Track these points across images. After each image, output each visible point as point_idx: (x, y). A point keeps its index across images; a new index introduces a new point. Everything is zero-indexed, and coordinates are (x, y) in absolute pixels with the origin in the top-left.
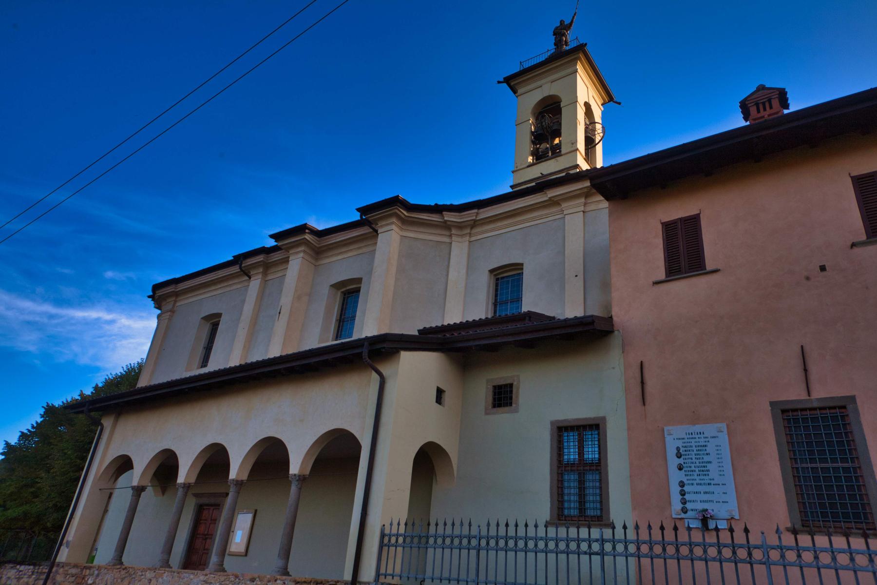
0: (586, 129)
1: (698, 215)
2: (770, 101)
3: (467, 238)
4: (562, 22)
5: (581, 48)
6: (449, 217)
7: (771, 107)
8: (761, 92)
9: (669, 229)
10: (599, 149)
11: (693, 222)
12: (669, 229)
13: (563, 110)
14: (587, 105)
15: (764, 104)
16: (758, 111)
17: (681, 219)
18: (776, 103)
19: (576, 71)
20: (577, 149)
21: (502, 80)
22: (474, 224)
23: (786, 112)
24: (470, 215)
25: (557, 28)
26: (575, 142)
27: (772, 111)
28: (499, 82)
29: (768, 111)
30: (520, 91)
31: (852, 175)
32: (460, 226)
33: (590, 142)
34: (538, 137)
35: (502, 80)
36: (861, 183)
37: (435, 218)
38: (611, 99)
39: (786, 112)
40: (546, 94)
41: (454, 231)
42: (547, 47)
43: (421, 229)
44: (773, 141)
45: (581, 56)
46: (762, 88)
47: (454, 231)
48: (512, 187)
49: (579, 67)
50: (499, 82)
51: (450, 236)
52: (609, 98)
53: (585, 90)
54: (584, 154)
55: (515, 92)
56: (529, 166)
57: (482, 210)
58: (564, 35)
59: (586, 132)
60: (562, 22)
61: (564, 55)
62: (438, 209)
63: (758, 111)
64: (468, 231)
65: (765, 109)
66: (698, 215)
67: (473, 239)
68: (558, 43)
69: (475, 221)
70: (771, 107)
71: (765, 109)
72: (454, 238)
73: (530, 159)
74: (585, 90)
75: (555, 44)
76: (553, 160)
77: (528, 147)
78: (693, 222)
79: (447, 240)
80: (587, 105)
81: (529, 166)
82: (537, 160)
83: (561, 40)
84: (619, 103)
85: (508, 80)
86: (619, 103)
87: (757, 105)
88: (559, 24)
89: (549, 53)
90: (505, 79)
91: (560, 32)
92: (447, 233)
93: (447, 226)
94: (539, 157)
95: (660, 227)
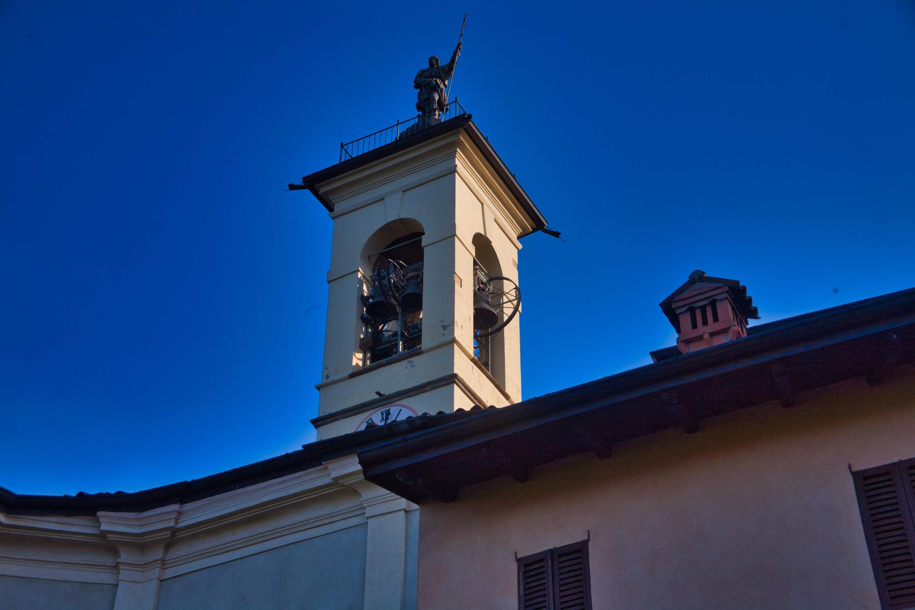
0: (478, 296)
1: (585, 543)
2: (713, 304)
3: (156, 572)
4: (432, 60)
5: (461, 122)
6: (112, 523)
7: (716, 319)
8: (696, 286)
9: (530, 567)
10: (512, 335)
11: (576, 555)
12: (530, 567)
13: (426, 252)
14: (482, 244)
15: (703, 309)
16: (695, 326)
17: (552, 552)
18: (726, 310)
19: (453, 171)
20: (454, 341)
21: (299, 182)
22: (173, 538)
23: (752, 323)
24: (162, 518)
25: (421, 74)
26: (448, 325)
27: (718, 326)
28: (292, 187)
29: (712, 326)
30: (339, 208)
31: (854, 469)
32: (140, 544)
33: (488, 323)
34: (375, 311)
35: (299, 182)
36: (872, 485)
37: (77, 526)
38: (538, 225)
39: (752, 323)
40: (392, 216)
41: (125, 556)
42: (406, 114)
43: (44, 555)
44: (717, 389)
45: (463, 138)
46: (698, 277)
47: (125, 556)
48: (317, 423)
49: (461, 163)
50: (292, 187)
51: (116, 567)
52: (534, 226)
53: (476, 209)
54: (471, 351)
55: (331, 209)
56: (353, 376)
57: (188, 506)
58: (436, 88)
59: (476, 296)
60: (432, 60)
61: (431, 135)
62: (84, 506)
63: (695, 326)
64: (158, 554)
65: (705, 323)
66: (585, 543)
67: (170, 573)
68: (425, 106)
69: (174, 531)
70: (716, 319)
71: (705, 323)
72: (124, 573)
73: (357, 359)
74: (476, 209)
75: (419, 107)
76: (404, 363)
77: (354, 329)
78: (576, 555)
79: (105, 577)
80: (482, 244)
81: (353, 376)
82: (373, 360)
83: (430, 100)
84: (557, 234)
85: (312, 183)
86: (557, 234)
87: (692, 311)
88: (426, 66)
89: (402, 129)
90: (305, 179)
91: (427, 84)
92: (109, 560)
93: (107, 545)
94: (380, 352)
95: (514, 567)
